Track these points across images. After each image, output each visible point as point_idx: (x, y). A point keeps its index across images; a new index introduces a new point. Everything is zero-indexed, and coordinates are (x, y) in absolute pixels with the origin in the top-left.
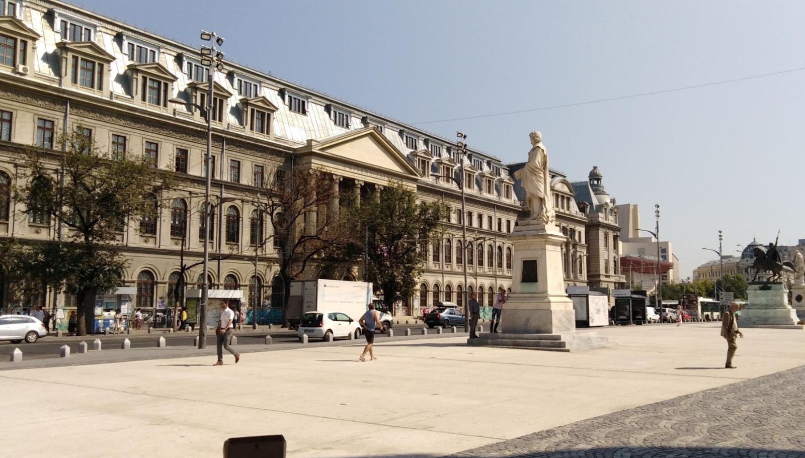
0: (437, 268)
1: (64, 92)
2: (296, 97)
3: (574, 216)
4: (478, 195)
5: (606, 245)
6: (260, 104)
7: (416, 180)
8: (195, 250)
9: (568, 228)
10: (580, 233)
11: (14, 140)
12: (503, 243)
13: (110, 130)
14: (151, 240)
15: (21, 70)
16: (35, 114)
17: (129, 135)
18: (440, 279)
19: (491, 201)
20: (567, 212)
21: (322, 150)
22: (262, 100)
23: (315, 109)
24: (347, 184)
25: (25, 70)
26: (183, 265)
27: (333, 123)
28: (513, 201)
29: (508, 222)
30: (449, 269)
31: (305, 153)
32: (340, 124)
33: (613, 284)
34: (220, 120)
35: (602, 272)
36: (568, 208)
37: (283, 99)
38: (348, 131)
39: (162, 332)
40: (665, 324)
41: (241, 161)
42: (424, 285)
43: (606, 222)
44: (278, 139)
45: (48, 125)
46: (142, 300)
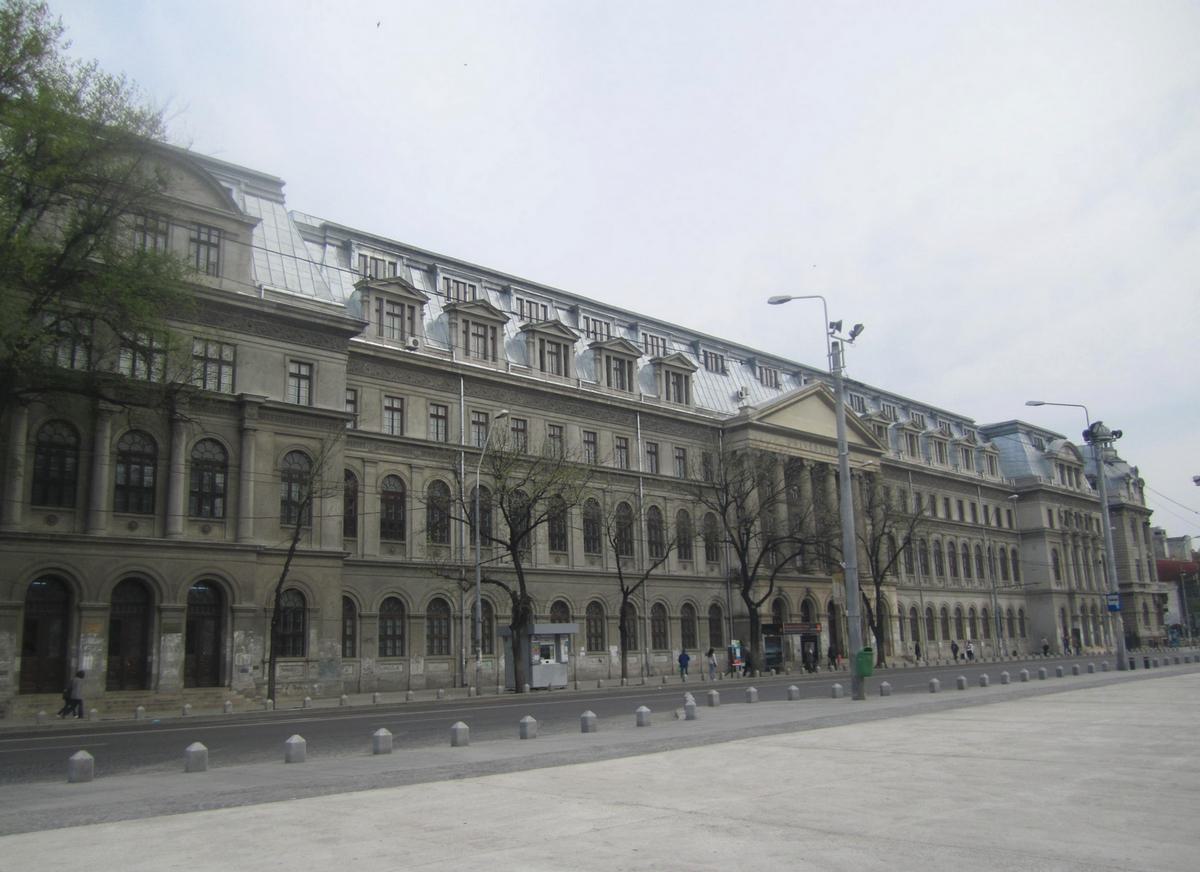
0: (912, 584)
1: (456, 366)
2: (712, 351)
3: (1085, 495)
4: (954, 472)
5: (1136, 538)
6: (617, 349)
7: (878, 455)
8: (581, 569)
9: (1083, 515)
10: (1098, 520)
11: (406, 435)
12: (943, 535)
13: (381, 390)
14: (563, 559)
15: (411, 344)
16: (545, 420)
17: (529, 417)
18: (917, 599)
19: (974, 480)
20: (1078, 491)
21: (758, 420)
22: (620, 343)
23: (733, 366)
24: (795, 465)
25: (415, 342)
26: (625, 588)
27: (759, 384)
28: (638, 398)
29: (986, 508)
30: (928, 585)
31: (741, 425)
32: (717, 370)
33: (1151, 597)
34: (631, 389)
35: (1134, 578)
36: (1079, 484)
37: (755, 374)
38: (780, 393)
39: (1114, 650)
40: (872, 703)
41: (528, 420)
42: (659, 607)
43: (1131, 503)
44: (698, 410)
45: (441, 412)
46: (443, 644)
